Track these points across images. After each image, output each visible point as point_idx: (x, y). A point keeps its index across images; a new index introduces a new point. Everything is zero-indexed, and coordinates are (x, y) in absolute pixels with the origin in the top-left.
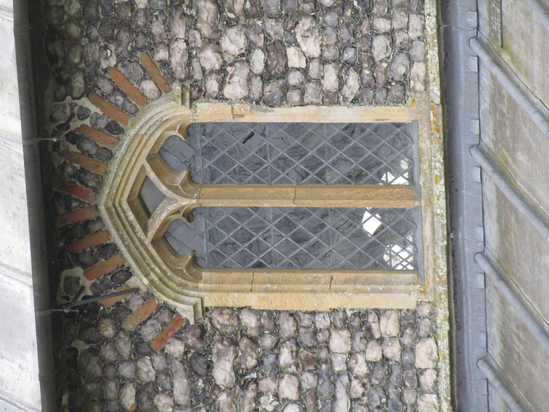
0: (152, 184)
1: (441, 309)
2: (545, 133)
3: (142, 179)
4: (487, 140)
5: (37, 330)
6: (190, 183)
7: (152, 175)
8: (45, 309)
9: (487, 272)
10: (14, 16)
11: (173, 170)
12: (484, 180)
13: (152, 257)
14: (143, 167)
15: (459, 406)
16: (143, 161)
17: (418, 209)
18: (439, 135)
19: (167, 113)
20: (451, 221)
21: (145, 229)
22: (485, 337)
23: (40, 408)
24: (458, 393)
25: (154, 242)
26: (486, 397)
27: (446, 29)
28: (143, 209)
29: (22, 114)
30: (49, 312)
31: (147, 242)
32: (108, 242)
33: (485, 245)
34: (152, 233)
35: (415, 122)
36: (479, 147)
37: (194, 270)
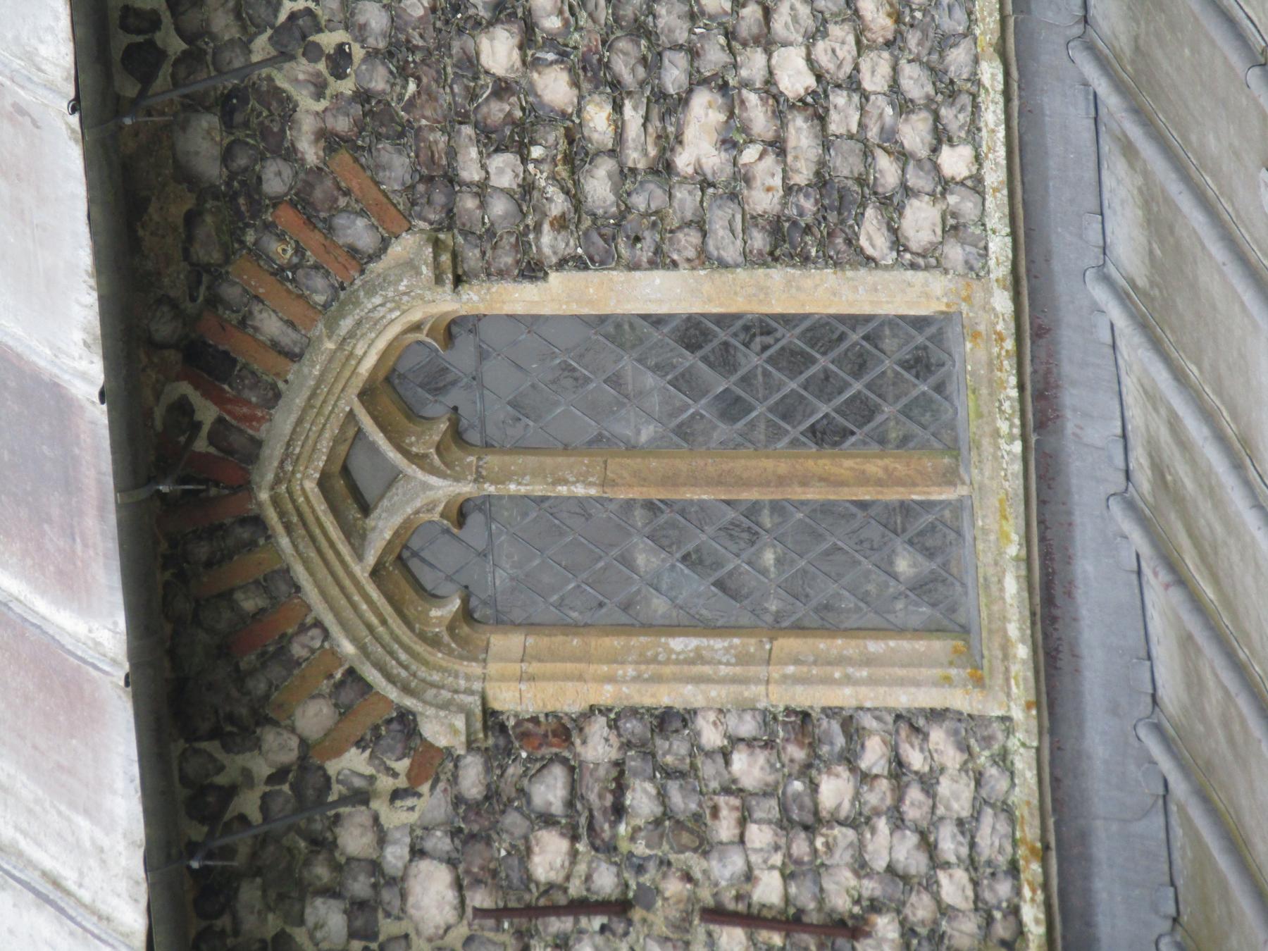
0: (373, 448)
1: (1023, 745)
2: (1242, 75)
5: (114, 452)
6: (455, 443)
8: (137, 486)
10: (99, 284)
17: (958, 507)
19: (403, 300)
20: (1049, 677)
23: (131, 916)
24: (1028, 270)
25: (375, 573)
28: (350, 493)
29: (105, 336)
30: (143, 493)
31: (361, 572)
32: (277, 567)
33: (1105, 254)
34: (371, 558)
37: (465, 630)
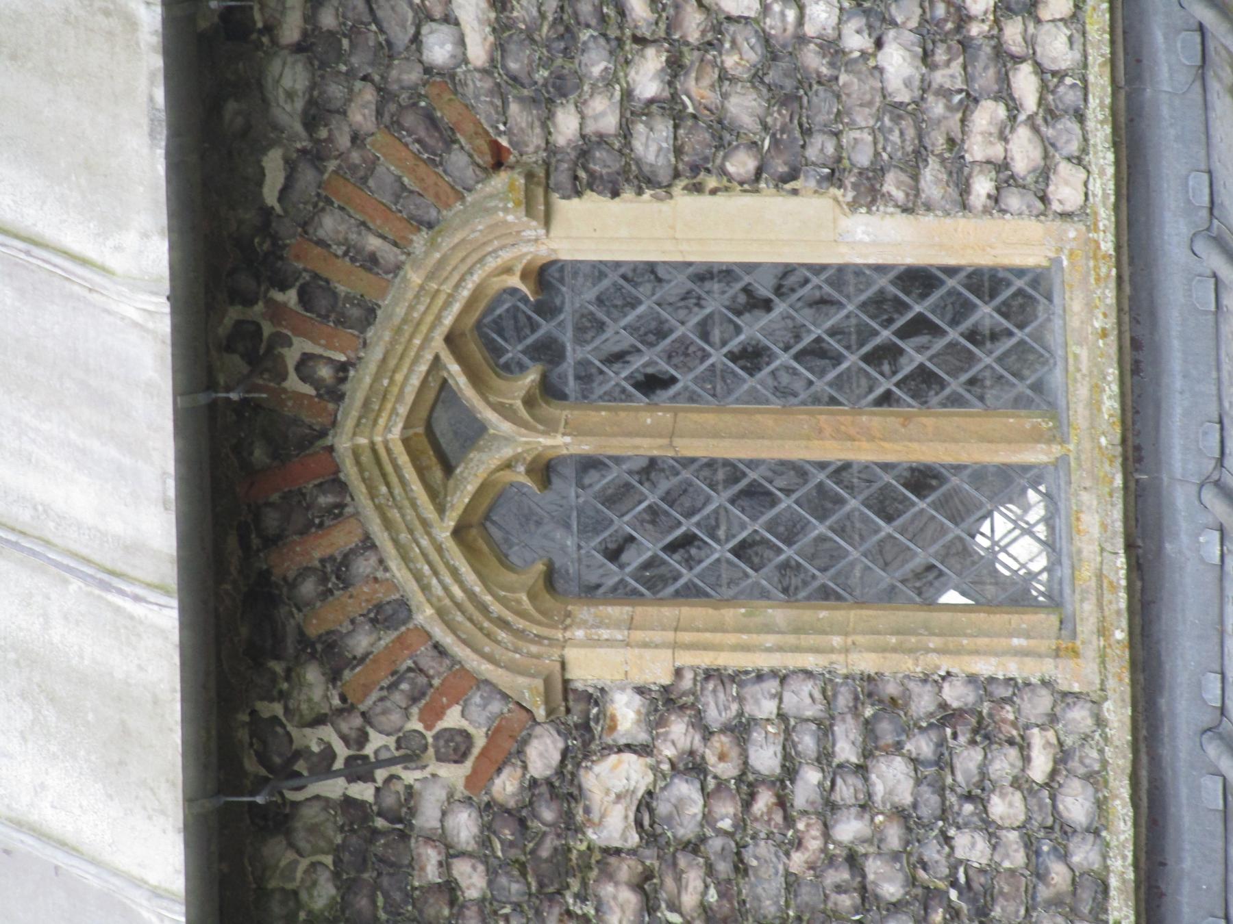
14: (437, 358)
26: (1218, 569)
28: (441, 441)
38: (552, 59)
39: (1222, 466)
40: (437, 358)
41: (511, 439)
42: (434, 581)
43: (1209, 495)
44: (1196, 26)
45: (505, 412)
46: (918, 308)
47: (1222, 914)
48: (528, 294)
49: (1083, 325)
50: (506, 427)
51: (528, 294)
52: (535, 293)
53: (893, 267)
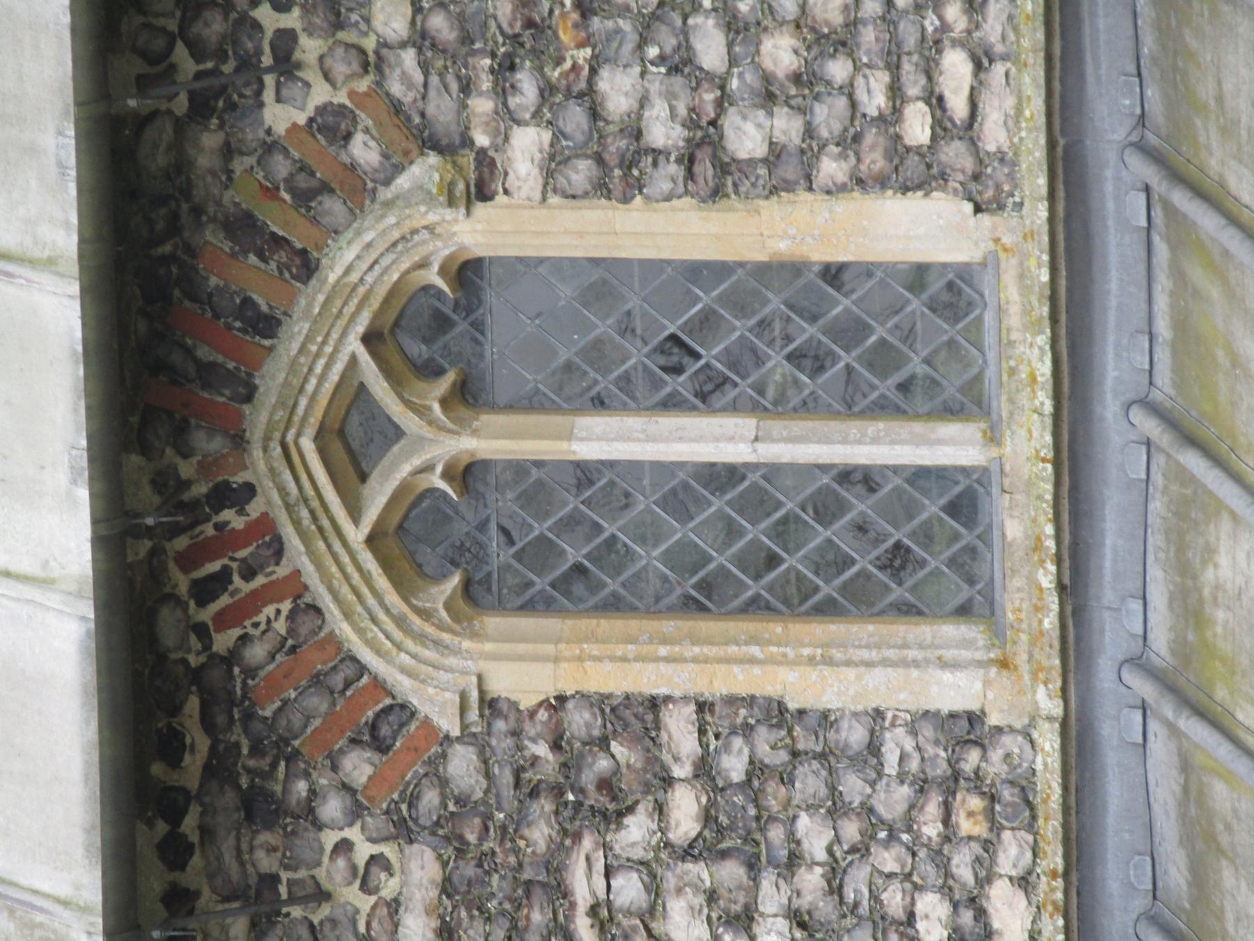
3: (351, 391)
4: (1160, 641)
7: (380, 388)
9: (1150, 700)
11: (422, 574)
12: (1151, 737)
13: (366, 577)
14: (353, 359)
15: (1079, 720)
16: (354, 345)
18: (1043, 92)
21: (355, 515)
22: (1141, 608)
25: (371, 541)
26: (1144, 234)
27: (1066, 150)
28: (354, 440)
31: (357, 535)
34: (371, 515)
35: (990, 263)
36: (1138, 662)
38: (467, 54)
39: (1144, 126)
40: (353, 359)
41: (429, 445)
42: (359, 609)
43: (1137, 415)
44: (1139, 703)
45: (421, 411)
46: (862, 507)
47: (1134, 71)
48: (446, 288)
49: (1022, 521)
50: (427, 432)
51: (446, 288)
52: (453, 291)
53: (832, 466)
